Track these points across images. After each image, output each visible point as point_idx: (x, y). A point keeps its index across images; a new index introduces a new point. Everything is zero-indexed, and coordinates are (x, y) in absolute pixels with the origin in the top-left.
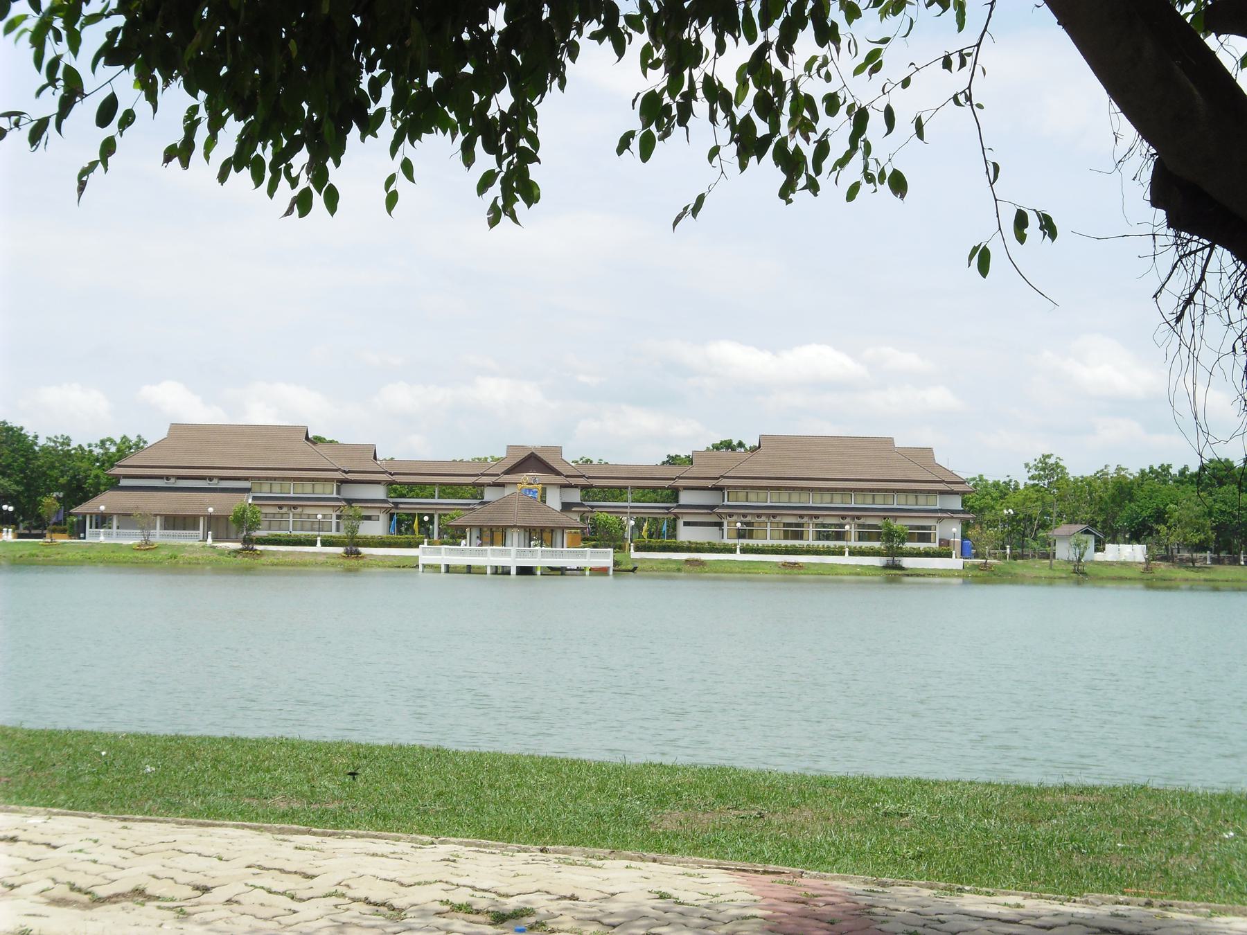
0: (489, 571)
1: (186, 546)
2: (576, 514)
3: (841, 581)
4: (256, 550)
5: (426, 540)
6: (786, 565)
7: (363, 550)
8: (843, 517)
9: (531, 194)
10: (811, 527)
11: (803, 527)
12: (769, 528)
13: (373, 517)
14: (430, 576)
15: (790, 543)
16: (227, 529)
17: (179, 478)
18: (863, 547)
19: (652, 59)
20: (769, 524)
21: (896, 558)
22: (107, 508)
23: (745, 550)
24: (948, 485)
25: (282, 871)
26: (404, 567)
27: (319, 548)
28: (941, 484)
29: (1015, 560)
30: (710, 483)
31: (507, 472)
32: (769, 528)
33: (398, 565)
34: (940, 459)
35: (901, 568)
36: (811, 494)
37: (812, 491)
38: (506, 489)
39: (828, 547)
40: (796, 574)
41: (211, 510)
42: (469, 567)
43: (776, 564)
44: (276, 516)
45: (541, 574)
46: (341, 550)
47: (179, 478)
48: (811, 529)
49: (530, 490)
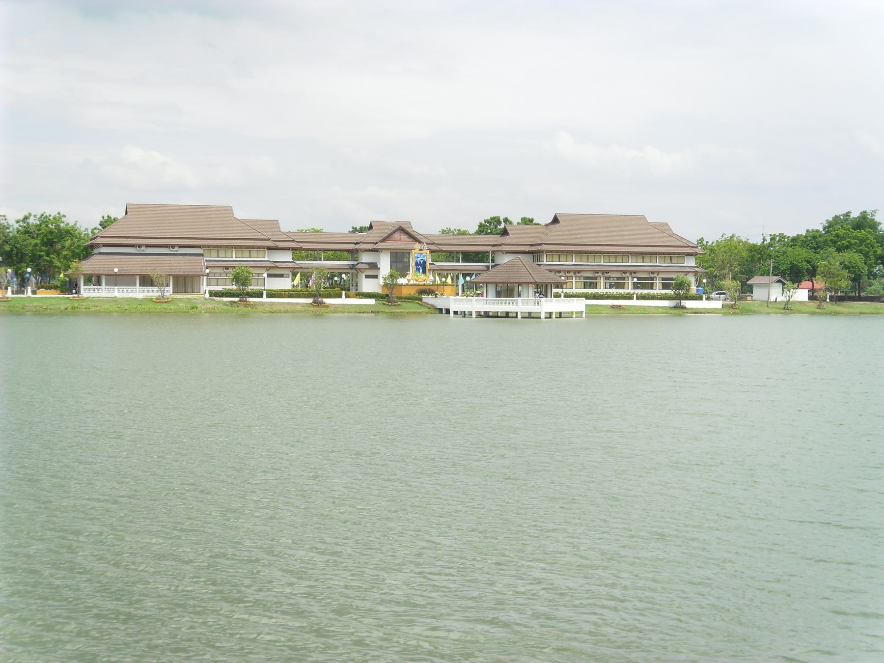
1: (90, 297)
2: (289, 270)
3: (650, 317)
4: (249, 302)
5: (344, 293)
6: (613, 307)
10: (658, 280)
11: (624, 280)
12: (574, 281)
13: (284, 276)
15: (614, 291)
16: (185, 284)
18: (643, 294)
20: (574, 278)
21: (682, 301)
22: (119, 271)
25: (825, 561)
26: (363, 313)
27: (265, 299)
28: (293, 243)
32: (574, 281)
33: (359, 311)
35: (684, 308)
36: (234, 251)
37: (603, 253)
38: (381, 253)
39: (620, 294)
40: (619, 313)
42: (507, 313)
43: (606, 306)
44: (222, 275)
45: (556, 318)
46: (310, 300)
48: (658, 282)
49: (421, 254)
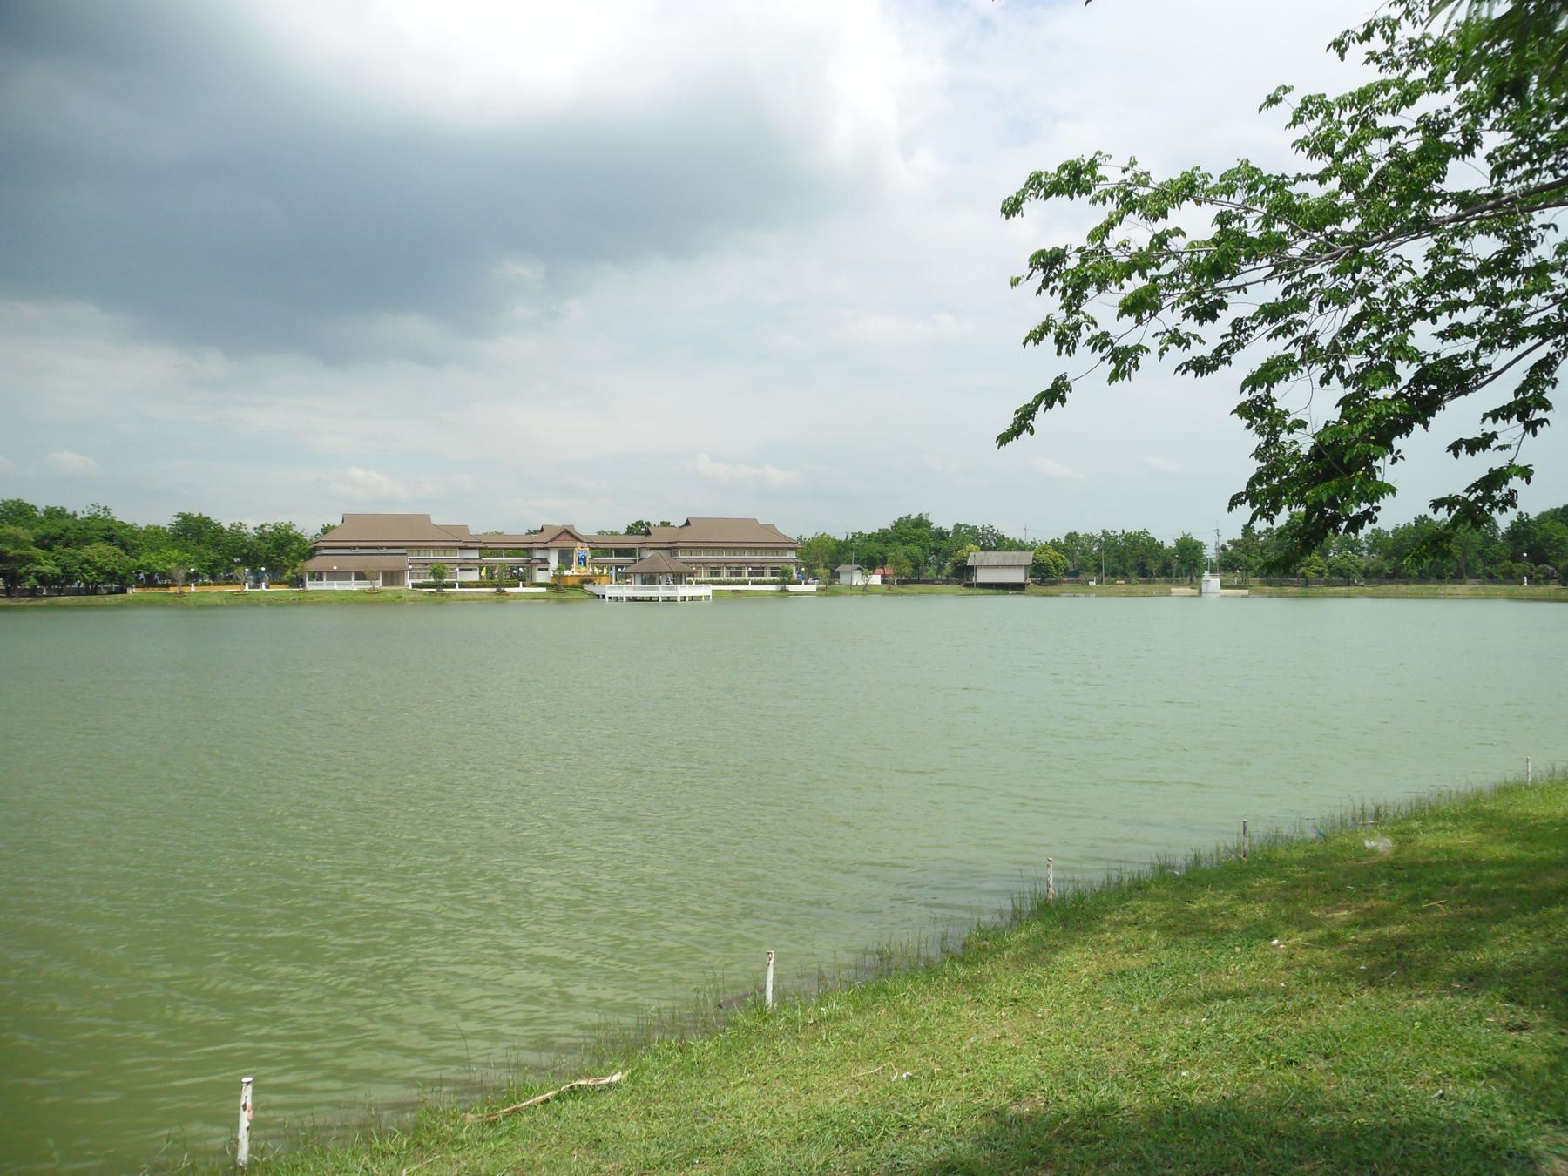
0: (679, 600)
6: (733, 591)
7: (507, 589)
8: (721, 563)
9: (1328, 383)
14: (613, 603)
15: (734, 578)
17: (388, 548)
19: (1508, 305)
23: (755, 583)
24: (786, 545)
29: (125, 592)
30: (665, 546)
31: (551, 541)
34: (780, 530)
41: (335, 568)
43: (728, 591)
46: (494, 590)
47: (388, 548)
